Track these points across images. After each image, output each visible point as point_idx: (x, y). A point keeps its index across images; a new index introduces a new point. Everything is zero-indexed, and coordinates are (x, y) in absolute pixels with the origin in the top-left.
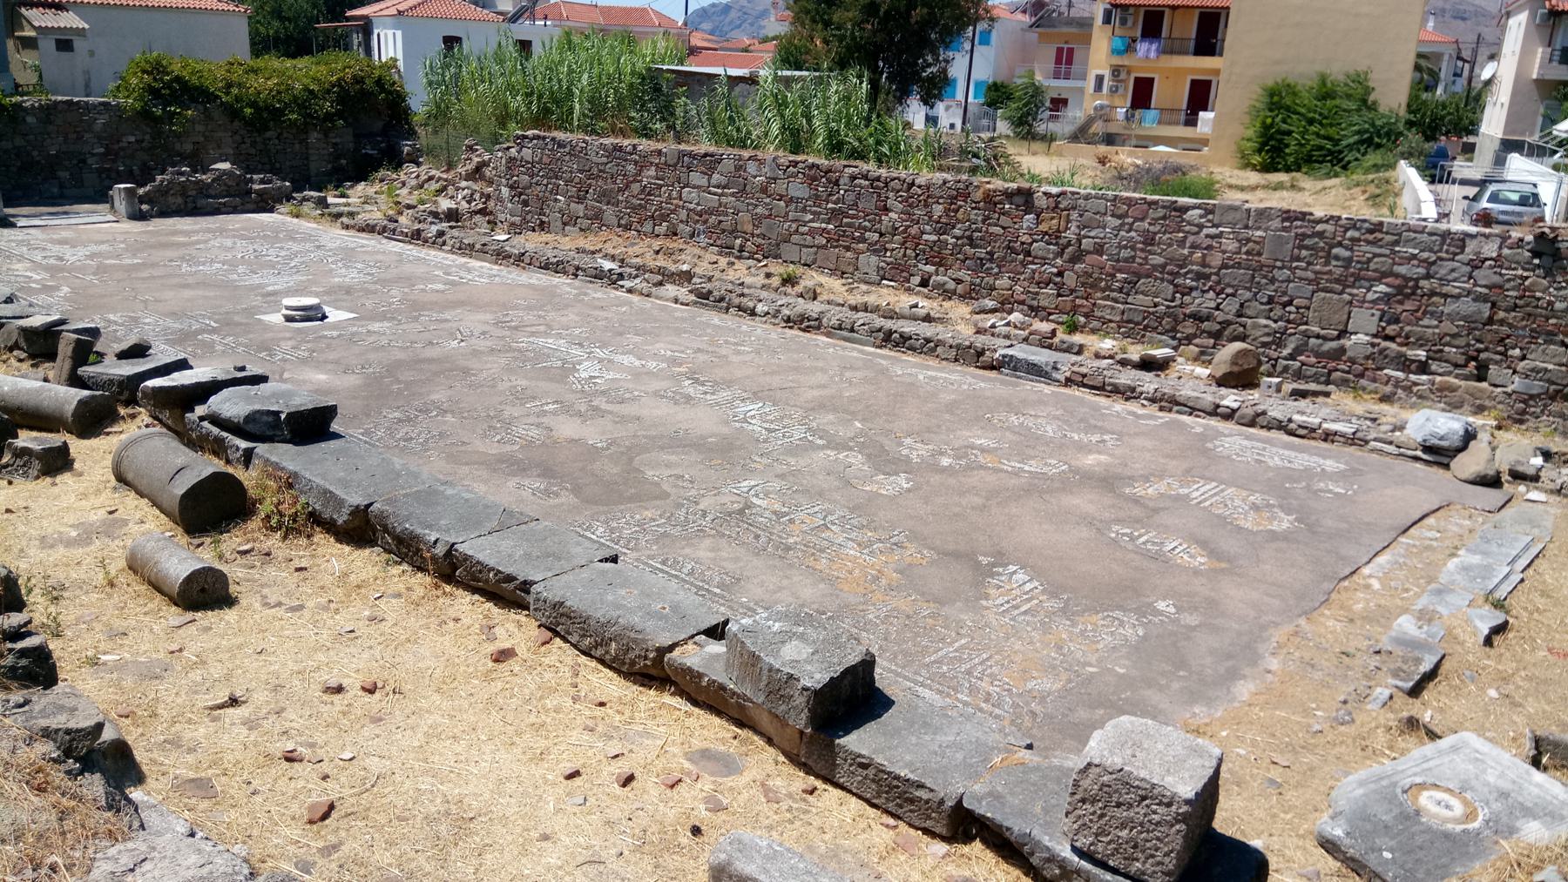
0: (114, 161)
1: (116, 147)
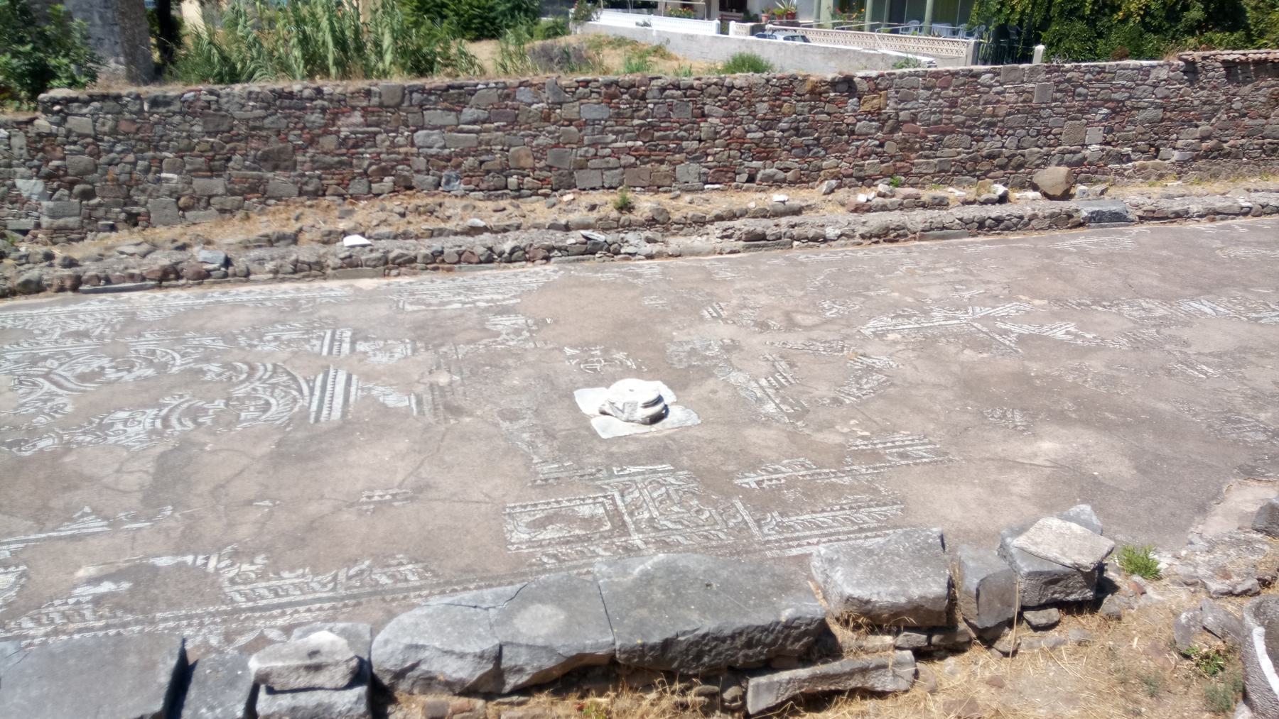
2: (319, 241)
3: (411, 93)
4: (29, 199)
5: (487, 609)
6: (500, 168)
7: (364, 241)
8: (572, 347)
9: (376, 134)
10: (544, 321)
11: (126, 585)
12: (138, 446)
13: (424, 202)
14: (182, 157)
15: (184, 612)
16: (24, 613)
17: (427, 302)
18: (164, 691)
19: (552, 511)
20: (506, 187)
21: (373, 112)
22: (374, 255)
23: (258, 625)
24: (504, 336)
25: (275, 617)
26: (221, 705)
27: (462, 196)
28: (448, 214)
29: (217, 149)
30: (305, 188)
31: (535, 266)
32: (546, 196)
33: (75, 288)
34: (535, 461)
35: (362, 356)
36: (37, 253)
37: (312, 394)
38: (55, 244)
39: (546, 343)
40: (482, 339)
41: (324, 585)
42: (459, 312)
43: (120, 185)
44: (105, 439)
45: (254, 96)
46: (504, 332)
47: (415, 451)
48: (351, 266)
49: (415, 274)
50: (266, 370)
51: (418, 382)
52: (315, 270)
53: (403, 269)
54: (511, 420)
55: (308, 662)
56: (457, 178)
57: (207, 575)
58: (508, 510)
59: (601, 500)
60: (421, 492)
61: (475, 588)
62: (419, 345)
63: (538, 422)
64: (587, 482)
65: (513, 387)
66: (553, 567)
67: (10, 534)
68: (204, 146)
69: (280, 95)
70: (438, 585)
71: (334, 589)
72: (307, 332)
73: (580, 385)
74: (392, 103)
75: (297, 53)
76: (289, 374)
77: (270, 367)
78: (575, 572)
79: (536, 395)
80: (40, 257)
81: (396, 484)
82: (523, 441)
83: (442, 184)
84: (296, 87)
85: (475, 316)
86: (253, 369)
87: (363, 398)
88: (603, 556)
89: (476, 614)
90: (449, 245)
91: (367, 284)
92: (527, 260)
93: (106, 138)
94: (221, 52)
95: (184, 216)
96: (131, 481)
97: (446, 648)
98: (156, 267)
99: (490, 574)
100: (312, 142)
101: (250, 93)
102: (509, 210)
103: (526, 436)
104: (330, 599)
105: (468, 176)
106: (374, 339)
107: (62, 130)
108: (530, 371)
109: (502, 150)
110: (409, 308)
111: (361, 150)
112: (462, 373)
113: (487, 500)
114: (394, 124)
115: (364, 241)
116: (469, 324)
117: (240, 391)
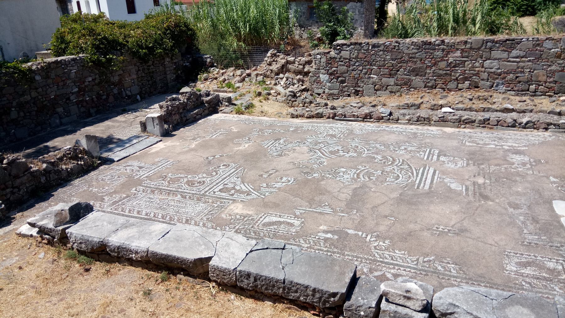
0: (84, 95)
1: (83, 86)
2: (429, 108)
3: (487, 42)
4: (323, 82)
5: (492, 299)
6: (527, 80)
7: (452, 111)
8: (554, 177)
9: (465, 61)
10: (540, 161)
11: (336, 237)
12: (347, 183)
13: (483, 95)
14: (380, 69)
15: (355, 254)
16: (301, 237)
17: (478, 142)
18: (347, 285)
19: (531, 260)
20: (528, 90)
21: (467, 51)
22: (455, 117)
23: (383, 269)
24: (516, 165)
25: (391, 269)
26: (367, 299)
27: (503, 93)
28: (494, 101)
29: (394, 66)
30: (428, 84)
31: (538, 132)
32: (550, 96)
33: (333, 118)
34: (525, 232)
35: (442, 163)
36: (323, 103)
37: (417, 176)
38: (328, 100)
39: (539, 173)
40: (504, 164)
41: (413, 262)
42: (493, 149)
43: (355, 79)
44: (336, 178)
45: (414, 44)
46: (517, 163)
47: (462, 212)
48: (443, 121)
49: (473, 128)
50: (399, 162)
51: (468, 180)
52: (426, 121)
53: (468, 125)
54: (514, 208)
55: (405, 294)
56: (502, 84)
57: (366, 242)
58: (506, 253)
59: (561, 262)
60: (462, 232)
61: (484, 286)
62: (470, 162)
63: (529, 212)
64: (554, 250)
65: (517, 192)
66: (527, 288)
67: (301, 206)
68: (390, 65)
69: (425, 43)
70: (466, 278)
71: (417, 264)
72: (419, 148)
73: (557, 198)
74: (476, 47)
75: (435, 24)
76: (409, 165)
77: (401, 161)
78: (540, 295)
79: (530, 198)
80: (323, 104)
81: (450, 226)
82: (519, 220)
83: (494, 86)
84: (433, 40)
85: (502, 153)
86: (394, 160)
87: (440, 182)
88: (558, 292)
89: (486, 300)
90: (493, 116)
91: (449, 130)
92: (534, 128)
93: (353, 60)
94: (402, 24)
95: (376, 93)
96: (343, 196)
97: (469, 311)
98: (363, 113)
99: (492, 282)
100: (435, 64)
101: (413, 42)
102: (528, 101)
103: (521, 218)
104: (414, 269)
105: (509, 83)
106: (449, 156)
107: (339, 56)
108: (528, 185)
109: (530, 71)
110: (467, 144)
111: (457, 68)
112: (491, 180)
113: (496, 245)
114: (475, 57)
115: (452, 111)
116: (498, 156)
117: (388, 169)
